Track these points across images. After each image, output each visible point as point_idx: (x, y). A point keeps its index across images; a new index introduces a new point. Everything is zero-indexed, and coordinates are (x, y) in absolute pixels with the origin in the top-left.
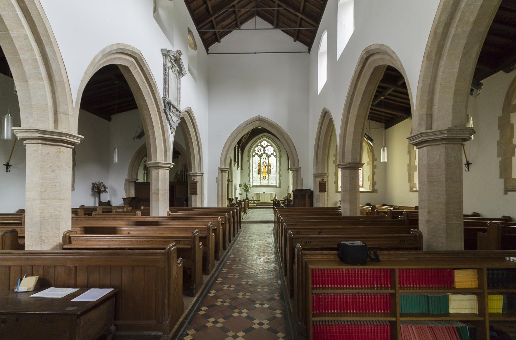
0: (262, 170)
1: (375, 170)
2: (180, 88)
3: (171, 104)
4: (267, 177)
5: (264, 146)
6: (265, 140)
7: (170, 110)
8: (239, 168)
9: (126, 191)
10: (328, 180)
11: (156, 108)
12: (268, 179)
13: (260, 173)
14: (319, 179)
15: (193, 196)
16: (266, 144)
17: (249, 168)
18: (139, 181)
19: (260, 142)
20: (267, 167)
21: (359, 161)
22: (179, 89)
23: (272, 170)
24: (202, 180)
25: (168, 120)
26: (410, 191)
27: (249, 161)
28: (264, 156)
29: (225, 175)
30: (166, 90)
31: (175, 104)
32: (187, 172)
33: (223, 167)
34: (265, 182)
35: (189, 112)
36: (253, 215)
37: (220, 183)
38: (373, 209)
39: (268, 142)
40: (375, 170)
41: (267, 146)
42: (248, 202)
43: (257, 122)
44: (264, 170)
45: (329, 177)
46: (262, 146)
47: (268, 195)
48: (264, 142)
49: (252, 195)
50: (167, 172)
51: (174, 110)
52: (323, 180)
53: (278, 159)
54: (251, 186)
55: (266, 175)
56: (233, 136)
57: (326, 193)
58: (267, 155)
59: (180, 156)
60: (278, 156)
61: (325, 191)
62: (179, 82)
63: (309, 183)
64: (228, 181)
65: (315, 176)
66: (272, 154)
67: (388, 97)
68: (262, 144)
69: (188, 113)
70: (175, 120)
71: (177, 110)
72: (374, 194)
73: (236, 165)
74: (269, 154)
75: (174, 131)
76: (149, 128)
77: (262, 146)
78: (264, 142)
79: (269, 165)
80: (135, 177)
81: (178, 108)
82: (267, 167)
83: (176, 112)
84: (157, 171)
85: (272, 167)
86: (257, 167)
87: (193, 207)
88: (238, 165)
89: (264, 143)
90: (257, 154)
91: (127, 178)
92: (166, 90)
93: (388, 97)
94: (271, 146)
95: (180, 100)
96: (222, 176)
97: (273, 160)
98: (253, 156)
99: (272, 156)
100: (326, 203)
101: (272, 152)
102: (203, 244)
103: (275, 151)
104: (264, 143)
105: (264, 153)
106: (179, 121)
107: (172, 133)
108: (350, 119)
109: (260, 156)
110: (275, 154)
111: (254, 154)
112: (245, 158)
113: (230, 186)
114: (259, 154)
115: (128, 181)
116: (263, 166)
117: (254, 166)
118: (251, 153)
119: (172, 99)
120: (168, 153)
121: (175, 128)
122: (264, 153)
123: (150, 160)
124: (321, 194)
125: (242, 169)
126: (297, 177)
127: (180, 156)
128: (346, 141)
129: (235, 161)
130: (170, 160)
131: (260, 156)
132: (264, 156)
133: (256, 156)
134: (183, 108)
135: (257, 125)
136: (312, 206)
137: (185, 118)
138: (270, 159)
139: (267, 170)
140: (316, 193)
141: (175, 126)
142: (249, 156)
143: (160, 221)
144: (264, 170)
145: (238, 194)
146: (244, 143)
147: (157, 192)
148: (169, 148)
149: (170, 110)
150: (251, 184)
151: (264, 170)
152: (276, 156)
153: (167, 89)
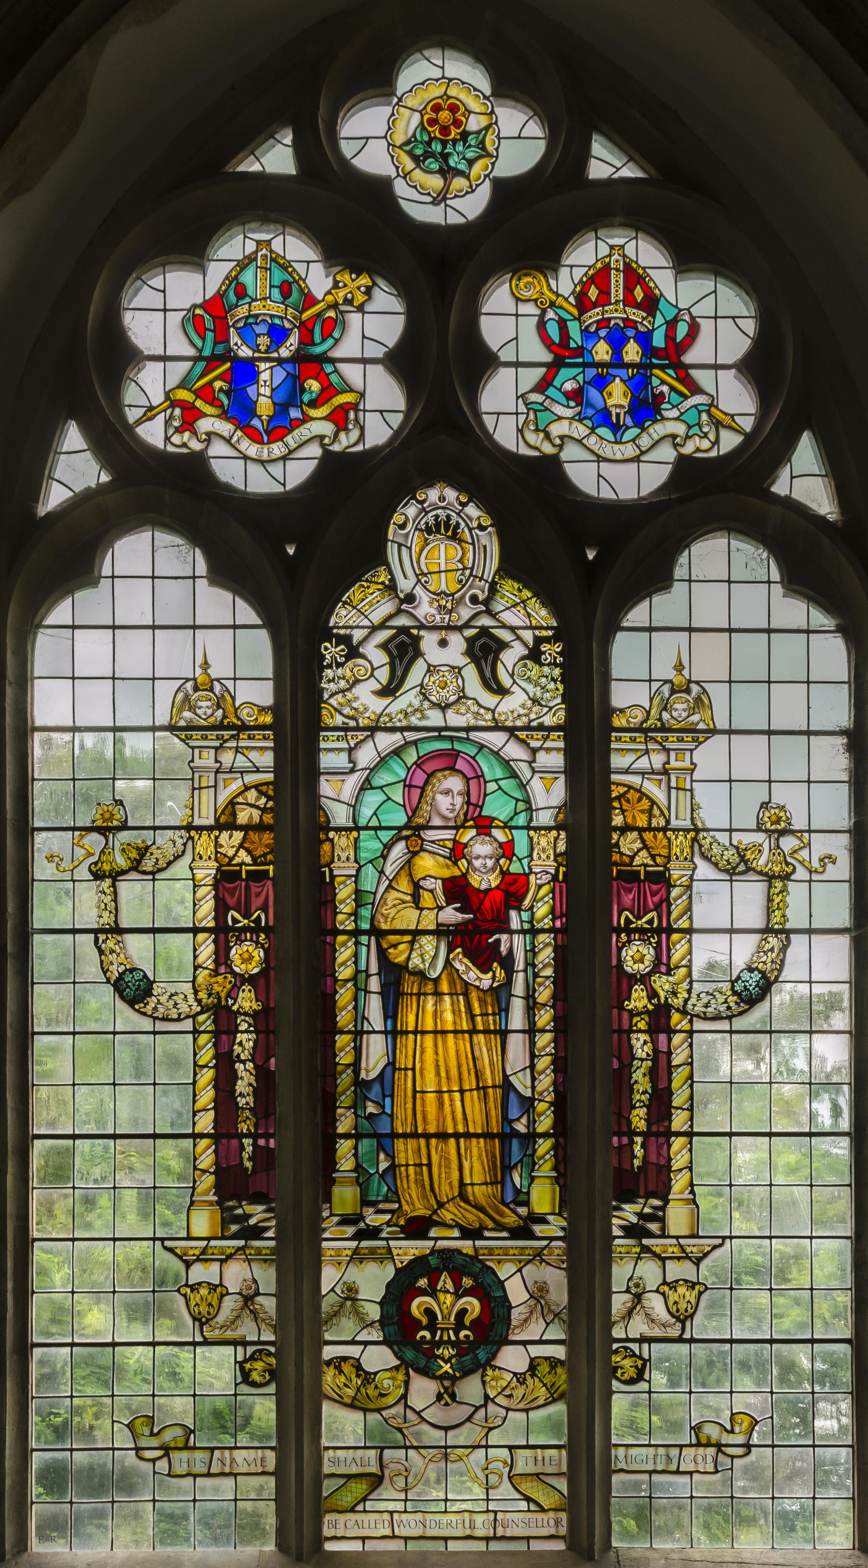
12: (590, 1367)
16: (518, 140)
20: (530, 942)
41: (531, 223)
46: (355, 222)
58: (536, 516)
66: (718, 494)
68: (370, 138)
77: (355, 222)
79: (610, 885)
85: (718, 928)
90: (164, 490)
99: (723, 580)
105: (443, 435)
109: (297, 560)
122: (443, 435)
133: (147, 565)
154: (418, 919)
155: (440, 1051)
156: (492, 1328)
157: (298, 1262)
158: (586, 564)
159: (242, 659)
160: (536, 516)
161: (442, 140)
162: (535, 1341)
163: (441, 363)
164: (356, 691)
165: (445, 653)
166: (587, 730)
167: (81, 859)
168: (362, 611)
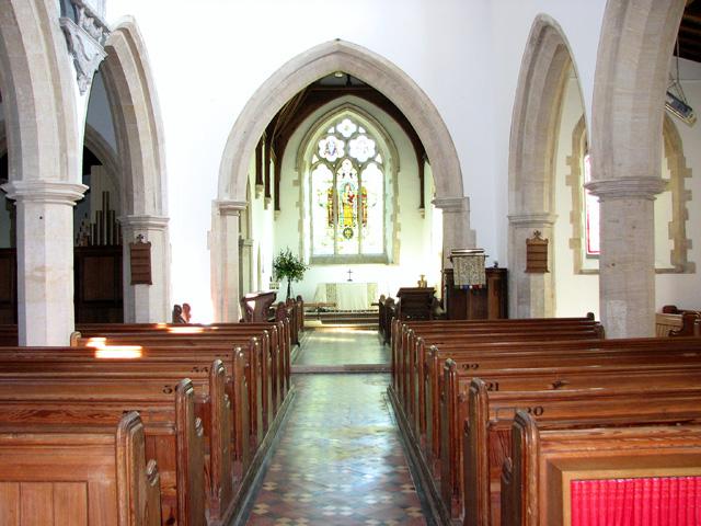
3: (84, 6)
4: (356, 231)
5: (347, 134)
6: (347, 117)
7: (77, 21)
10: (552, 235)
11: (37, 17)
14: (529, 233)
15: (139, 288)
16: (353, 128)
19: (335, 124)
28: (347, 166)
29: (232, 220)
34: (349, 248)
39: (359, 124)
41: (355, 135)
43: (333, 57)
44: (347, 213)
45: (556, 225)
46: (340, 137)
48: (347, 122)
52: (538, 234)
53: (389, 176)
58: (355, 162)
61: (544, 270)
63: (496, 247)
65: (516, 223)
66: (371, 160)
68: (340, 128)
69: (126, 31)
70: (93, 53)
71: (98, 24)
72: (686, 277)
73: (262, 194)
74: (362, 159)
75: (89, 87)
77: (340, 137)
78: (347, 122)
79: (362, 196)
81: (99, 14)
82: (355, 200)
83: (94, 30)
84: (37, 209)
86: (325, 200)
87: (139, 320)
88: (267, 195)
90: (325, 161)
94: (368, 134)
97: (374, 179)
98: (314, 167)
99: (372, 167)
101: (372, 153)
103: (378, 150)
104: (347, 126)
105: (347, 156)
106: (101, 58)
107: (82, 92)
109: (335, 166)
110: (379, 159)
113: (245, 259)
114: (332, 159)
118: (306, 158)
121: (91, 76)
124: (533, 277)
125: (277, 207)
129: (259, 181)
131: (335, 166)
132: (347, 166)
133: (322, 167)
134: (112, 20)
138: (364, 173)
140: (518, 276)
141: (90, 68)
142: (299, 167)
147: (39, 274)
148: (74, 140)
149: (77, 21)
151: (345, 209)
152: (381, 166)
154: (346, 199)
163: (347, 149)
164: (339, 178)
165: (347, 175)
166: (360, 182)
167: (339, 244)
168: (340, 171)
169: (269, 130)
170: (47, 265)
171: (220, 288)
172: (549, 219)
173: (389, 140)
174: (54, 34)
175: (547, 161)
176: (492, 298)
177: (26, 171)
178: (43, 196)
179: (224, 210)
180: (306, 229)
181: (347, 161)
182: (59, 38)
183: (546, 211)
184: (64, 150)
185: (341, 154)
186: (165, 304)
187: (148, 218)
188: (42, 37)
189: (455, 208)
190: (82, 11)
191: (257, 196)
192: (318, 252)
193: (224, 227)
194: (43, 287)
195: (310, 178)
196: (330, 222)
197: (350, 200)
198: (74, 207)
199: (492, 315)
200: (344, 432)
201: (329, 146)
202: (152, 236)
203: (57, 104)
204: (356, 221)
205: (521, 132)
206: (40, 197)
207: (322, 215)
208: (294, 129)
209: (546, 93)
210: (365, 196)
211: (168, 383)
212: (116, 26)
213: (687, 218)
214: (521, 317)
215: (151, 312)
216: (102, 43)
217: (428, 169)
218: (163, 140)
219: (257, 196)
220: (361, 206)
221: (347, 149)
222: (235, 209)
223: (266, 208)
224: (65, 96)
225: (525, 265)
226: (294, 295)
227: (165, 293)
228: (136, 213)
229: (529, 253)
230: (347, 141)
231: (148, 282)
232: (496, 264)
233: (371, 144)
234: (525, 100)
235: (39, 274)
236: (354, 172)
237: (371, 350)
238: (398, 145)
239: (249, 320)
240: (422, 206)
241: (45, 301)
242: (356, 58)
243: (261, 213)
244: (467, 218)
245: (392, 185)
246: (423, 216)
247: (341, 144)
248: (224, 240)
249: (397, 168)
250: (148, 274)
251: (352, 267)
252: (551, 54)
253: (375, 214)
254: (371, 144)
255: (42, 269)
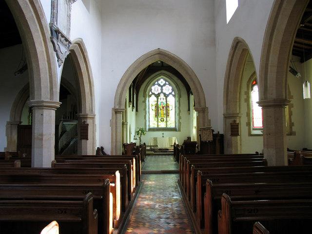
0: (160, 112)
1: (292, 109)
2: (70, 15)
3: (60, 33)
4: (165, 119)
5: (162, 84)
6: (162, 78)
7: (57, 38)
8: (134, 110)
9: (7, 135)
10: (240, 122)
11: (41, 36)
12: (167, 121)
13: (157, 115)
14: (230, 121)
15: (83, 141)
16: (164, 82)
17: (145, 109)
18: (22, 124)
19: (158, 81)
20: (165, 108)
21: (284, 97)
22: (69, 16)
23: (170, 112)
24: (94, 122)
25: (56, 51)
26: (179, 130)
27: (145, 102)
28: (162, 96)
29: (120, 116)
30: (54, 15)
31: (65, 33)
32: (76, 113)
33: (117, 107)
34: (162, 125)
35: (80, 44)
36: (151, 163)
37: (114, 126)
38: (295, 154)
39: (166, 81)
40: (292, 109)
41: (165, 85)
42: (145, 147)
43: (157, 55)
44: (162, 112)
45: (242, 118)
46: (159, 85)
47: (169, 141)
48: (162, 80)
49: (148, 139)
50: (53, 113)
51: (63, 39)
52: (235, 121)
53: (177, 99)
54: (147, 130)
55: (164, 117)
56: (129, 72)
57: (238, 137)
58: (165, 94)
59: (68, 96)
60: (177, 95)
61: (238, 135)
62: (70, 9)
63: (219, 126)
64: (123, 124)
65: (226, 117)
66: (170, 93)
67: (308, 24)
68: (160, 82)
69: (79, 45)
70: (64, 52)
71: (67, 40)
72: (292, 137)
73: (131, 106)
74: (167, 93)
75: (63, 64)
76: (33, 60)
77: (159, 85)
78: (162, 80)
79: (167, 106)
80: (18, 119)
81: (67, 37)
82: (165, 108)
83: (65, 42)
84: (40, 111)
85: (170, 109)
86: (154, 108)
87: (83, 154)
88: (133, 106)
89: (162, 82)
90: (154, 94)
91: (9, 120)
92: (54, 15)
93: (308, 24)
94: (170, 84)
95: (69, 29)
96: (116, 118)
97: (172, 100)
98: (150, 96)
99: (171, 96)
100: (239, 149)
101: (170, 91)
102: (98, 212)
103: (173, 90)
104: (162, 82)
105: (162, 92)
106: (68, 53)
107: (59, 66)
108: (272, 47)
109: (158, 96)
110: (173, 93)
111: (151, 93)
112: (141, 99)
113: (125, 129)
114: (156, 93)
115: (10, 125)
116: (160, 106)
117: (150, 107)
118: (147, 93)
119: (61, 26)
120: (54, 90)
121: (64, 60)
122: (162, 92)
123: (33, 98)
124: (233, 138)
125: (137, 110)
126: (204, 118)
127: (68, 96)
128: (269, 73)
129: (130, 101)
130: (57, 98)
131: (158, 96)
132: (162, 96)
133: (153, 96)
134: (73, 38)
135: (157, 59)
136: (223, 153)
137: (75, 50)
138: (168, 98)
139: (165, 112)
140: (228, 135)
141: (63, 58)
142: (145, 96)
143: (43, 174)
144: (162, 111)
145: (131, 138)
146: (138, 84)
147: (40, 137)
148: (56, 85)
149: (57, 38)
150: (147, 128)
151: (162, 111)
152: (174, 96)
153: (55, 15)
154: (161, 108)
155: (204, 160)
156: (163, 121)
157: (158, 118)
158: (166, 96)
159: (156, 99)
160: (165, 94)
161: (162, 82)
162: (165, 120)
163: (162, 90)
164: (159, 100)
165: (162, 99)
166: (166, 101)
167: (159, 123)
168: (159, 98)
169: (134, 82)
170: (44, 133)
171: (206, 114)
172: (239, 115)
173: (177, 86)
174: (48, 44)
175: (238, 94)
176: (218, 145)
177: (36, 97)
178: (87, 117)
179: (116, 112)
180: (147, 119)
181: (162, 94)
182: (50, 45)
183: (238, 112)
184: (51, 88)
185: (160, 91)
186: (93, 147)
187: (43, 102)
188: (43, 44)
189: (202, 111)
190: (60, 35)
191: (129, 106)
192: (152, 126)
193: (116, 118)
194: (42, 143)
195: (149, 100)
196: (156, 116)
197: (163, 108)
198: (56, 111)
199: (218, 153)
200: (160, 192)
201: (155, 89)
202: (89, 121)
203: (49, 70)
204: (165, 116)
205: (228, 82)
206: (41, 106)
207: (152, 113)
208: (143, 82)
209: (238, 69)
210: (168, 106)
211: (85, 190)
212: (74, 42)
213: (292, 115)
214: (229, 154)
215: (88, 150)
216: (68, 47)
217: (192, 97)
218: (93, 85)
219: (129, 106)
220: (167, 111)
221: (162, 90)
222: (120, 112)
223: (133, 111)
224: (52, 67)
225: (230, 132)
226: (142, 143)
227: (94, 143)
228: (83, 113)
229: (231, 128)
230: (162, 87)
231: (87, 139)
232: (219, 132)
233: (171, 88)
234: (230, 70)
235: (40, 137)
236: (164, 98)
237: (169, 163)
238: (180, 88)
239: (126, 153)
240: (189, 110)
241: (43, 148)
242: (165, 55)
243: (131, 114)
244: (207, 115)
245: (178, 103)
246: (189, 114)
247: (160, 88)
248: (116, 123)
249: (180, 96)
250: (87, 136)
251: (164, 132)
252: (240, 52)
253: (172, 113)
254: (171, 88)
255: (42, 135)
